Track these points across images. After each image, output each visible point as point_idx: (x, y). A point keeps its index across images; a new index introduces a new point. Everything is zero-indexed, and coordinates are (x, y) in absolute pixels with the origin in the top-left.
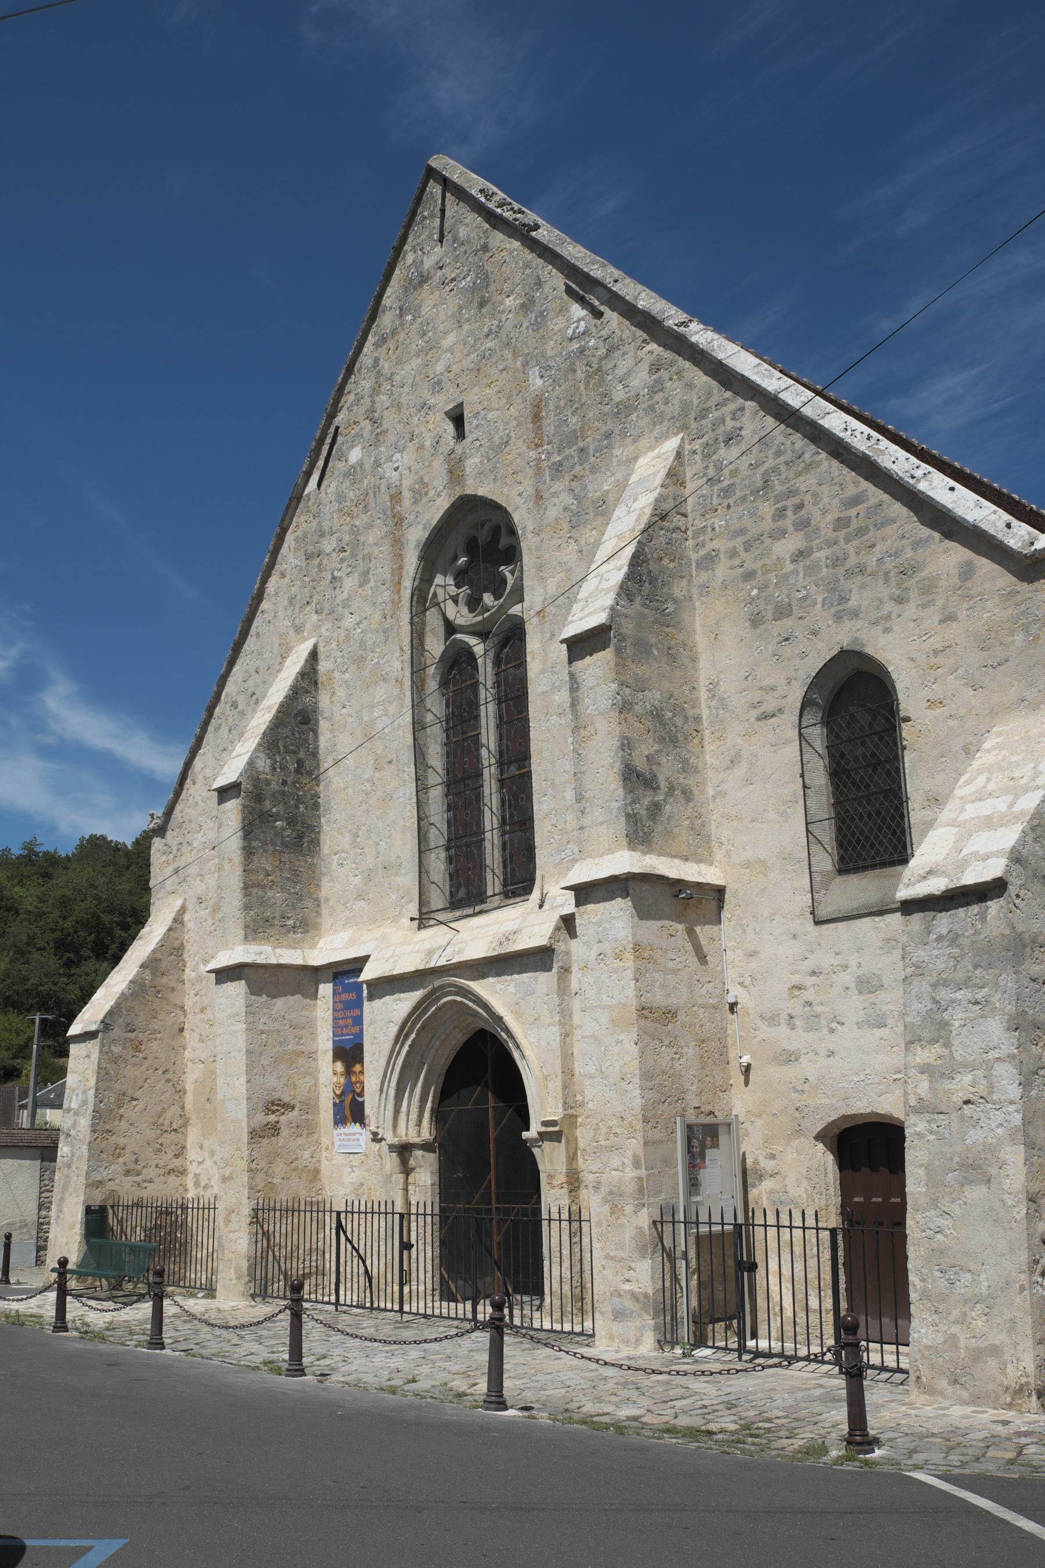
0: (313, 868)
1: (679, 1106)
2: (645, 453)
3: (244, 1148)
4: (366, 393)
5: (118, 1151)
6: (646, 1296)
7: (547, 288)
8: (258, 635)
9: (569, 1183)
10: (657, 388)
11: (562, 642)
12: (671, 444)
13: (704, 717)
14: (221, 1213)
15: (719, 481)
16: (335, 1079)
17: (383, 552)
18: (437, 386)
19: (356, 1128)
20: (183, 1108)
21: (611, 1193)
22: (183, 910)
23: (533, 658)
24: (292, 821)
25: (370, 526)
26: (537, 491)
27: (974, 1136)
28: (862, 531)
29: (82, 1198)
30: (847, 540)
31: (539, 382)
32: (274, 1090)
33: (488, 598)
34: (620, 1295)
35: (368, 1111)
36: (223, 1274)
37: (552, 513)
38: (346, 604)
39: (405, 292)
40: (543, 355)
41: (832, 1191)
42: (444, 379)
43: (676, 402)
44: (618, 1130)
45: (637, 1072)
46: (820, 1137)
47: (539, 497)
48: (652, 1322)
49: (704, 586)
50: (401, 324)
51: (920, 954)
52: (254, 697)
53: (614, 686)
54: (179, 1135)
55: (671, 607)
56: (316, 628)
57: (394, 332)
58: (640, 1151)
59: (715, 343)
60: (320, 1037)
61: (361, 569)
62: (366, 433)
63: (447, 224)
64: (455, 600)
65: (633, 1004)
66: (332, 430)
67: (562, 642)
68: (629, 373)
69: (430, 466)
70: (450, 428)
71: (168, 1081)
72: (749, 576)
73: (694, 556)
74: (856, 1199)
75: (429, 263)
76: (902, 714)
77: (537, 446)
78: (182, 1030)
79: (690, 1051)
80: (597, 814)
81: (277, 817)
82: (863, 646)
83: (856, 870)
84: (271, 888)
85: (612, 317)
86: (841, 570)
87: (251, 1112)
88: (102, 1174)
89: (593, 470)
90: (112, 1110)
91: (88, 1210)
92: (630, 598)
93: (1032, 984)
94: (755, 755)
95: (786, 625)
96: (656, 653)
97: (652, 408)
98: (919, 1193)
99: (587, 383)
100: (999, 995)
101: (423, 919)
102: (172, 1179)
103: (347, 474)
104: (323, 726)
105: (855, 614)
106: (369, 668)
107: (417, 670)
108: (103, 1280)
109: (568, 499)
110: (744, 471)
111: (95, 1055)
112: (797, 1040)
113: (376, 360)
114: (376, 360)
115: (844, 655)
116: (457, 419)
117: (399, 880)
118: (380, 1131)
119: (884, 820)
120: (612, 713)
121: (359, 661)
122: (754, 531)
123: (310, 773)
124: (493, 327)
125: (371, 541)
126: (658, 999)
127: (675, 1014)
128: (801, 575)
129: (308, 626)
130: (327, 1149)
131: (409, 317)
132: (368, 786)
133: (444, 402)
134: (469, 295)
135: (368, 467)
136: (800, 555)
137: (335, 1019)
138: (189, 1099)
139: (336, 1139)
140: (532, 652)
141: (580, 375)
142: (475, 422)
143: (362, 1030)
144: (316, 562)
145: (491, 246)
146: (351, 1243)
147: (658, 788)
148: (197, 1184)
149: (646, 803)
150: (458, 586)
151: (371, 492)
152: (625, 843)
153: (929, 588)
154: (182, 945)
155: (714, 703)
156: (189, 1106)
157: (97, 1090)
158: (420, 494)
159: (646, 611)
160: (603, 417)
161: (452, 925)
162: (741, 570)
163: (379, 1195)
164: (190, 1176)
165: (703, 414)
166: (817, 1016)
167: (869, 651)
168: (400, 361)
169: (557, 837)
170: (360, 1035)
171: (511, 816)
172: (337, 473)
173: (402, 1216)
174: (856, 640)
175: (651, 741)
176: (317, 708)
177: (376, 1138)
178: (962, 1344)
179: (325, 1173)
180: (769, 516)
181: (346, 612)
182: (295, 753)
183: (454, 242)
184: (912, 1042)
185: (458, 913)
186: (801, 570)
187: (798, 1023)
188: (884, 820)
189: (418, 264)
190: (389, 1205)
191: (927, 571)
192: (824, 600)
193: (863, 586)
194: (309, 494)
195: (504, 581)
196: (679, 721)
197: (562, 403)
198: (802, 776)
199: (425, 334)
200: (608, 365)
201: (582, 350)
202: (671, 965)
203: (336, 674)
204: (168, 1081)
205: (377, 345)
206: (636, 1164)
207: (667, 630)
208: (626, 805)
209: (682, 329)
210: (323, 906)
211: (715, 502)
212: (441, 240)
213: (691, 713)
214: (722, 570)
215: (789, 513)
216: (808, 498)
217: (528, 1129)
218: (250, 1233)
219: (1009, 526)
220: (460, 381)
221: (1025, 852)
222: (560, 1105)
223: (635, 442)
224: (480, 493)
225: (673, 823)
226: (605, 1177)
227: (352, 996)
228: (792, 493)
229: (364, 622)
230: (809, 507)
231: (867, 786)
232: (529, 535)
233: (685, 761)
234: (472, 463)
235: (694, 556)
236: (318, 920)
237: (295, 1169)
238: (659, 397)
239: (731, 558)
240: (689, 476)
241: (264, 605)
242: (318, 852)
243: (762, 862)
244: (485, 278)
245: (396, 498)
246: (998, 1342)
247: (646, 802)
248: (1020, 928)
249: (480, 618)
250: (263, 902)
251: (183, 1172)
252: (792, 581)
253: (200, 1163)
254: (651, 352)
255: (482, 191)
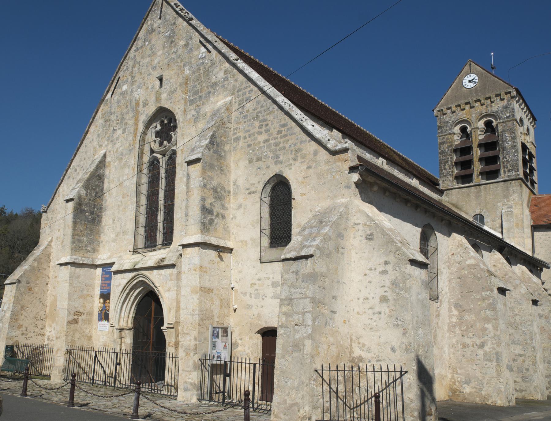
0: (98, 230)
1: (211, 321)
2: (220, 101)
3: (65, 327)
4: (131, 67)
5: (20, 327)
6: (195, 384)
7: (194, 41)
8: (86, 146)
9: (175, 345)
10: (226, 79)
11: (185, 162)
12: (228, 99)
13: (231, 191)
14: (55, 350)
15: (243, 113)
16: (100, 305)
17: (131, 122)
18: (154, 68)
19: (105, 322)
20: (45, 311)
21: (186, 349)
22: (51, 241)
23: (178, 165)
24: (92, 213)
25: (128, 113)
26: (185, 109)
27: (297, 336)
28: (285, 136)
29: (5, 342)
30: (281, 138)
31: (188, 72)
32: (78, 307)
33: (165, 142)
34: (186, 383)
35: (110, 317)
36: (54, 371)
37: (189, 117)
38: (117, 139)
39: (147, 34)
40: (191, 62)
41: (259, 351)
42: (157, 66)
43: (232, 85)
44: (190, 328)
45: (198, 309)
46: (258, 332)
47: (185, 111)
48: (196, 392)
49: (234, 148)
50: (145, 45)
51: (287, 276)
52: (83, 168)
53: (201, 179)
54: (43, 322)
55: (223, 154)
56: (106, 146)
57: (141, 47)
58: (197, 335)
59: (245, 67)
60: (96, 290)
61: (123, 128)
62: (129, 80)
63: (162, 13)
64: (155, 141)
65: (199, 286)
66: (117, 78)
67: (185, 162)
68: (217, 73)
69: (150, 95)
70: (158, 82)
71: (41, 302)
72: (249, 146)
73: (233, 137)
74: (267, 355)
75: (155, 26)
76: (293, 197)
77: (186, 93)
78: (47, 284)
79: (217, 303)
80: (191, 221)
81: (86, 211)
82: (283, 173)
83: (272, 247)
84: (82, 236)
85: (214, 52)
86: (278, 148)
87: (69, 313)
88: (13, 334)
89: (203, 104)
90: (19, 311)
91: (7, 347)
92: (209, 149)
93: (319, 288)
94: (246, 205)
95: (260, 163)
96: (216, 169)
97: (224, 86)
98: (280, 353)
99: (204, 75)
100: (308, 291)
101: (135, 251)
102: (39, 337)
103: (121, 94)
104: (106, 181)
105: (281, 163)
106: (123, 162)
107: (140, 165)
108: (10, 372)
109: (193, 112)
110: (251, 111)
111: (14, 291)
112: (252, 301)
113: (135, 56)
114: (135, 56)
115: (277, 176)
116: (161, 79)
117: (128, 237)
118: (113, 324)
119: (285, 231)
120: (199, 188)
121: (120, 159)
122: (252, 132)
123: (100, 197)
124: (175, 51)
125: (128, 118)
126: (207, 285)
127: (212, 290)
128: (266, 147)
129: (104, 145)
130: (95, 329)
131: (147, 43)
132: (120, 203)
133: (157, 74)
134: (168, 39)
135: (129, 92)
136: (266, 141)
137: (102, 284)
138: (48, 309)
139: (98, 326)
140: (178, 163)
141: (202, 71)
142: (166, 82)
143: (110, 288)
144: (108, 123)
145: (176, 23)
146: (99, 362)
147: (213, 214)
148: (48, 339)
149: (208, 219)
150: (156, 137)
151: (129, 101)
152: (200, 232)
153: (304, 157)
154: (50, 254)
155: (235, 187)
156: (47, 311)
157: (14, 304)
158: (146, 104)
159: (214, 154)
160: (208, 87)
161: (144, 254)
162: (247, 143)
163: (112, 346)
164: (46, 336)
165: (239, 91)
166: (259, 294)
167: (284, 175)
168: (143, 57)
169: (181, 227)
170: (110, 290)
171: (167, 218)
172: (118, 93)
173: (117, 353)
174: (281, 171)
175: (212, 198)
176: (104, 174)
177: (112, 325)
178: (288, 402)
179: (94, 338)
180: (257, 127)
181: (117, 142)
182: (95, 189)
183: (164, 20)
184: (282, 305)
185: (146, 250)
186: (266, 146)
187: (253, 296)
188: (285, 231)
189: (152, 25)
190: (92, 349)
191: (304, 151)
192: (272, 157)
193: (284, 154)
194: (108, 99)
195: (172, 137)
196: (222, 192)
197: (195, 80)
198: (260, 214)
199: (152, 49)
200: (211, 69)
201: (203, 63)
202: (213, 273)
203: (112, 163)
204: (41, 302)
205: (136, 51)
206: (195, 339)
207: (221, 161)
208: (201, 219)
209: (235, 61)
210: (101, 244)
211: (241, 120)
212: (160, 19)
213: (227, 189)
214: (241, 143)
215: (264, 126)
216: (270, 123)
217: (163, 326)
218: (65, 357)
219: (329, 140)
220: (162, 67)
221: (320, 246)
222: (174, 318)
223: (217, 96)
224: (166, 106)
225: (217, 226)
226: (185, 343)
227: (108, 276)
228: (266, 120)
229: (123, 146)
230: (270, 125)
231: (281, 219)
232: (181, 123)
233: (223, 206)
234: (164, 96)
235: (233, 137)
236: (99, 249)
237: (83, 336)
238: (226, 82)
239: (244, 139)
240: (233, 110)
241: (88, 135)
242: (101, 225)
243: (246, 242)
244: (173, 34)
245: (138, 104)
246: (298, 402)
247: (209, 218)
248: (317, 270)
249: (162, 149)
250: (79, 241)
251: (44, 335)
252: (263, 149)
253: (50, 332)
254: (225, 67)
255: (175, 4)
